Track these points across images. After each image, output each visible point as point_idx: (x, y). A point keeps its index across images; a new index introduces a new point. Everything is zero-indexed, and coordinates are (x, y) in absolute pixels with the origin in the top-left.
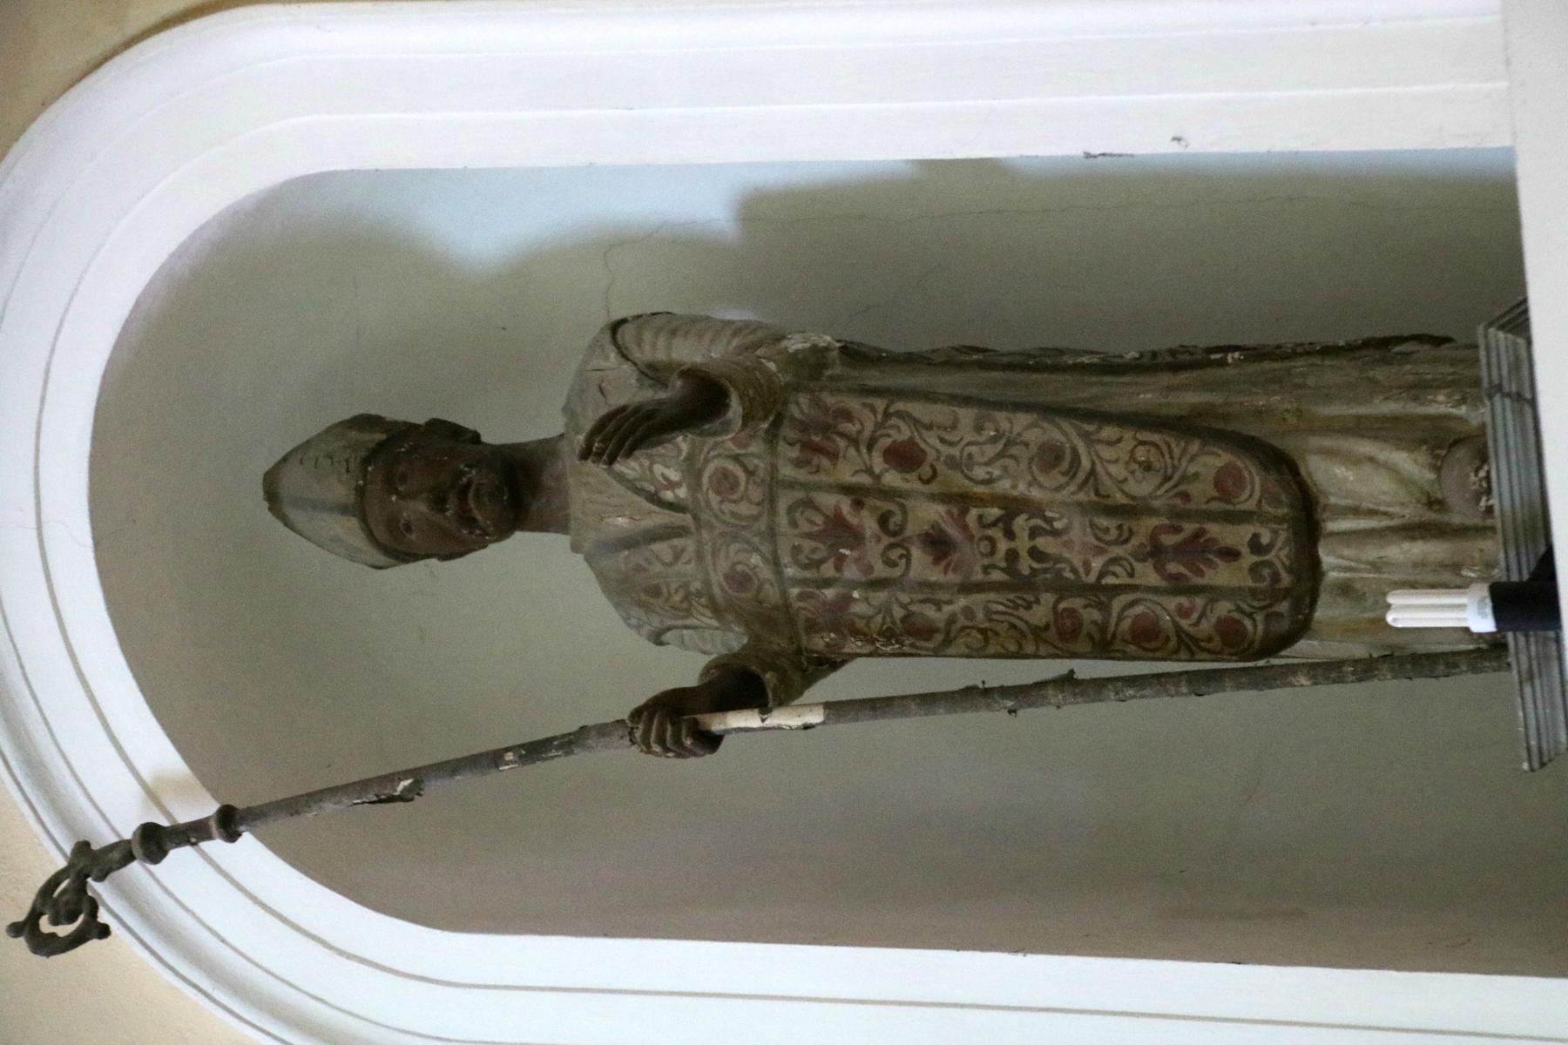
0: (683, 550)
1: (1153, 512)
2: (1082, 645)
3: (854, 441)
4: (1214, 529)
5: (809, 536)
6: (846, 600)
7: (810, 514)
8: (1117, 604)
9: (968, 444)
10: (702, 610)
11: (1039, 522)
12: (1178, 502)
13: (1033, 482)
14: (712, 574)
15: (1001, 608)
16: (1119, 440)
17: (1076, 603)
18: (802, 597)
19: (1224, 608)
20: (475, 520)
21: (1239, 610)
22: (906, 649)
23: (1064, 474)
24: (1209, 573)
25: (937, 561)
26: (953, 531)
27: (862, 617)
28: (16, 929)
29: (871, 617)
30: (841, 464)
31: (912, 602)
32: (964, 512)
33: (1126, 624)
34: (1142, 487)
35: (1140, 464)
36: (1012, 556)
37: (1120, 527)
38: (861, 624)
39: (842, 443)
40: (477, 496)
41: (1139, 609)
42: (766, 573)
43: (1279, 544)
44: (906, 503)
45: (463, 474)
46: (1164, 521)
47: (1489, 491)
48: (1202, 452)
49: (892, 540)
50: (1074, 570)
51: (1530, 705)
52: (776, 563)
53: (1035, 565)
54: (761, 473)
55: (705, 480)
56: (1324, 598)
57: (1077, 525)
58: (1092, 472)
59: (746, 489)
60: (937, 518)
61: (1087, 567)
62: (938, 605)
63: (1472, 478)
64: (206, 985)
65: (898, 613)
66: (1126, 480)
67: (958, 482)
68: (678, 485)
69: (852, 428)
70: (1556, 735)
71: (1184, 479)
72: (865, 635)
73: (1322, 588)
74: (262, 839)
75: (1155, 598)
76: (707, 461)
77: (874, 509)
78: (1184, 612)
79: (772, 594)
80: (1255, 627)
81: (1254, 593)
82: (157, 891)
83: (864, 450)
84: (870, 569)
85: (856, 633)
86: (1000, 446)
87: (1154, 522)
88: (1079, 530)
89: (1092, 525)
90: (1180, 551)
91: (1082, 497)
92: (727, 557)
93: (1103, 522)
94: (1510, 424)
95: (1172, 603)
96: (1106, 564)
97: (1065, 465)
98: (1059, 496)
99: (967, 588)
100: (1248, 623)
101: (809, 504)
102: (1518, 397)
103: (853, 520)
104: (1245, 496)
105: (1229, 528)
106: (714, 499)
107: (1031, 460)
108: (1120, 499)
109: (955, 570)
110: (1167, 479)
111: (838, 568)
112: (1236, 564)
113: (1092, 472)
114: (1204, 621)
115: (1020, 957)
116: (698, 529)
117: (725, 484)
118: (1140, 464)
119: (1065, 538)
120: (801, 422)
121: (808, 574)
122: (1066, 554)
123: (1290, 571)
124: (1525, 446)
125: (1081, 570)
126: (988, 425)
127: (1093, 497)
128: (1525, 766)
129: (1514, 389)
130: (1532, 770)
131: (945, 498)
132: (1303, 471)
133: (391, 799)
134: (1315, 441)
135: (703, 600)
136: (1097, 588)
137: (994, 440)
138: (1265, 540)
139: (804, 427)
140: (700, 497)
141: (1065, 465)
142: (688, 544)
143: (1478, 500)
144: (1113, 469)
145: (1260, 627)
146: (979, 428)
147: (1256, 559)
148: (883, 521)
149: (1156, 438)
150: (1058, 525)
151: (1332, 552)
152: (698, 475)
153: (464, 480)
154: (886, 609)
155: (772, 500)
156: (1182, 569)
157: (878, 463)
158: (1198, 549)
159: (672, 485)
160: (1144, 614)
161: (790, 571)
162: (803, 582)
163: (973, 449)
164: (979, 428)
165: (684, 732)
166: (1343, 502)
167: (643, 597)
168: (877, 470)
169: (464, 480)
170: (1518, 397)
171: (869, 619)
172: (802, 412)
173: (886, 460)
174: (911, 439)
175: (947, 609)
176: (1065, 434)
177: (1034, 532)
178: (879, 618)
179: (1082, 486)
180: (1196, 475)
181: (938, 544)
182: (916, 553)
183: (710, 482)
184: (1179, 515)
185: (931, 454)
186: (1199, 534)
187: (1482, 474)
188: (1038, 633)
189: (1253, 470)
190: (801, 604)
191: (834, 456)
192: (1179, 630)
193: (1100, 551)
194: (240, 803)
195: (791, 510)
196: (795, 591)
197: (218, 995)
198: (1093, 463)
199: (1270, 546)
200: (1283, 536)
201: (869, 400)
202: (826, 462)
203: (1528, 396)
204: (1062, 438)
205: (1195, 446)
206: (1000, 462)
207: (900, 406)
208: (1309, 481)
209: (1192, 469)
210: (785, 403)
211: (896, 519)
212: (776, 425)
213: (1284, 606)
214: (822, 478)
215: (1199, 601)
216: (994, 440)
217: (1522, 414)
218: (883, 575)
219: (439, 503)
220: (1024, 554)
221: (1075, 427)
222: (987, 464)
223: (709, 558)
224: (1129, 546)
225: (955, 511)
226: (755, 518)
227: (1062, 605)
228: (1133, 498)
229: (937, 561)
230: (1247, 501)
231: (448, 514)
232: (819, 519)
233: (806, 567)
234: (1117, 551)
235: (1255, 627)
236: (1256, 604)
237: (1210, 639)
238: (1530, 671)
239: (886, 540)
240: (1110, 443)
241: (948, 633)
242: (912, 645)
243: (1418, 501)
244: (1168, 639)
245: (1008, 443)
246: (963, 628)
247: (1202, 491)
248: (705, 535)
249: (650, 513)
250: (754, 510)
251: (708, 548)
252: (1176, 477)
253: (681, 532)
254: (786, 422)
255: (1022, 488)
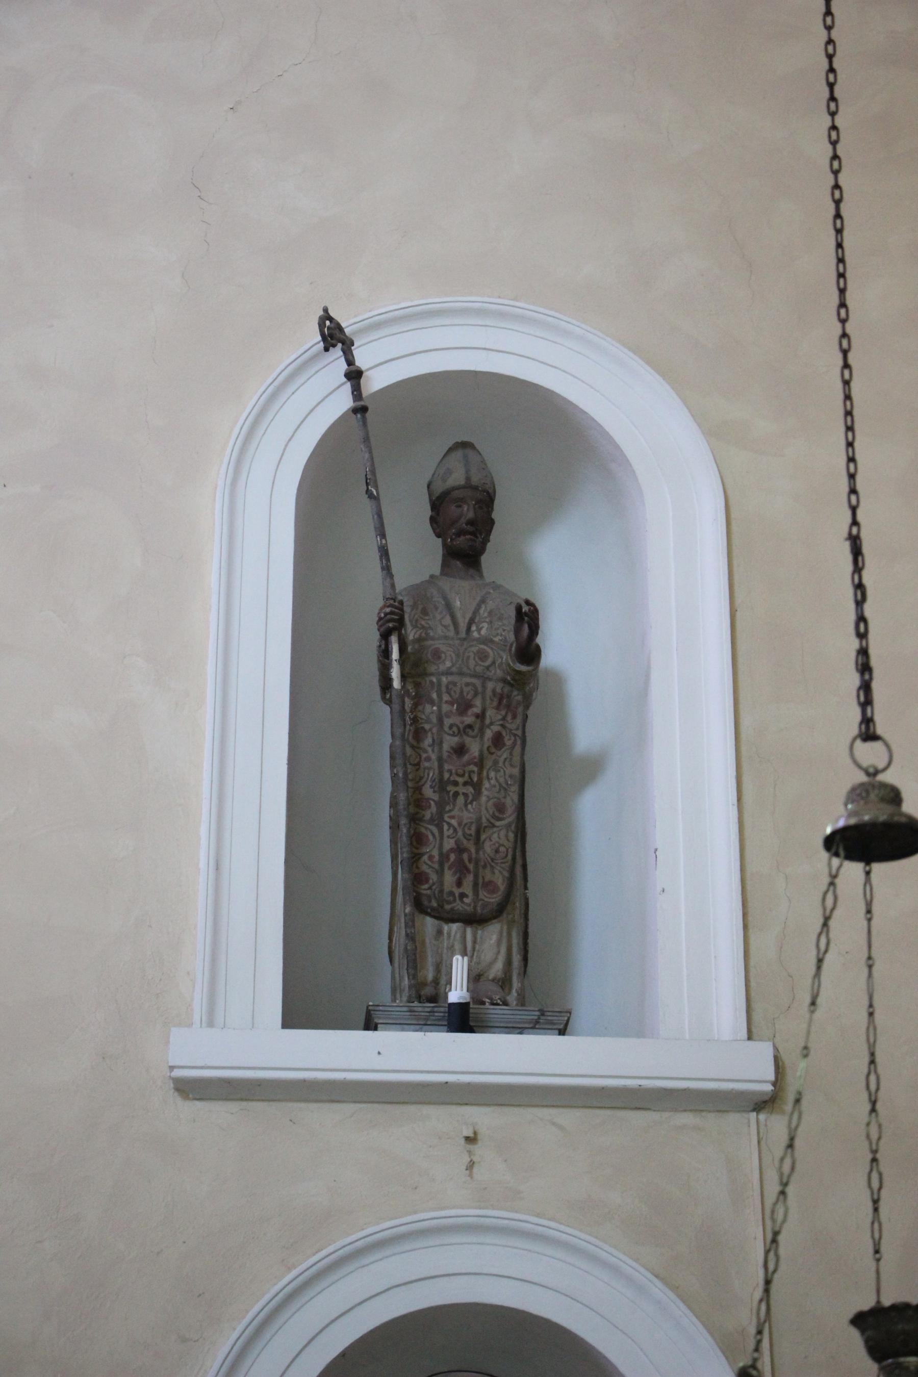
1: (477, 852)
2: (412, 809)
3: (504, 719)
4: (470, 878)
5: (462, 692)
6: (432, 703)
8: (435, 830)
10: (418, 633)
11: (471, 798)
12: (483, 864)
13: (489, 799)
15: (431, 775)
17: (434, 809)
19: (434, 877)
20: (459, 536)
21: (434, 884)
22: (408, 727)
24: (451, 872)
25: (452, 748)
26: (466, 758)
28: (326, 310)
29: (424, 713)
30: (494, 711)
32: (475, 764)
33: (423, 830)
34: (488, 848)
36: (456, 784)
37: (471, 835)
38: (420, 708)
39: (503, 713)
40: (471, 540)
41: (431, 837)
42: (442, 668)
45: (481, 534)
46: (474, 856)
50: (450, 811)
51: (398, 1009)
52: (448, 673)
53: (451, 793)
54: (488, 673)
55: (482, 646)
56: (436, 922)
57: (471, 815)
58: (494, 826)
61: (452, 817)
62: (432, 745)
64: (276, 383)
65: (427, 727)
67: (488, 763)
68: (479, 632)
69: (509, 718)
75: (437, 846)
76: (492, 649)
78: (431, 858)
81: (441, 891)
82: (316, 368)
83: (501, 722)
84: (448, 717)
86: (504, 785)
87: (473, 850)
88: (468, 816)
89: (472, 823)
90: (460, 861)
93: (473, 828)
95: (435, 853)
97: (497, 814)
98: (483, 809)
99: (440, 760)
100: (426, 886)
102: (537, 1022)
103: (470, 712)
105: (471, 884)
106: (475, 649)
107: (499, 799)
108: (483, 837)
109: (449, 756)
110: (493, 860)
112: (454, 885)
113: (494, 826)
116: (460, 639)
117: (483, 656)
121: (444, 689)
122: (456, 809)
123: (452, 909)
128: (371, 1003)
131: (482, 758)
133: (367, 484)
134: (505, 927)
135: (423, 635)
136: (442, 819)
138: (465, 900)
139: (509, 697)
141: (497, 814)
142: (452, 633)
144: (495, 835)
145: (424, 892)
146: (511, 776)
147: (457, 895)
148: (470, 727)
150: (469, 806)
152: (484, 643)
154: (428, 721)
155: (475, 675)
157: (496, 728)
158: (461, 869)
159: (479, 630)
160: (429, 840)
161: (444, 680)
162: (439, 684)
164: (511, 776)
167: (420, 607)
170: (537, 1022)
175: (430, 749)
178: (423, 717)
179: (488, 820)
180: (494, 873)
181: (460, 750)
185: (499, 753)
186: (468, 871)
191: (498, 708)
192: (422, 855)
193: (460, 824)
195: (474, 685)
196: (434, 680)
197: (272, 387)
199: (463, 902)
201: (521, 728)
207: (519, 742)
209: (496, 871)
210: (518, 690)
211: (470, 732)
212: (509, 683)
214: (488, 702)
215: (436, 866)
216: (507, 784)
217: (530, 1023)
219: (471, 523)
220: (456, 789)
222: (496, 778)
224: (462, 838)
226: (468, 668)
227: (432, 803)
229: (452, 748)
230: (483, 894)
232: (469, 697)
233: (447, 687)
234: (460, 833)
237: (417, 867)
239: (461, 726)
240: (507, 836)
241: (419, 748)
244: (417, 849)
245: (505, 789)
248: (457, 642)
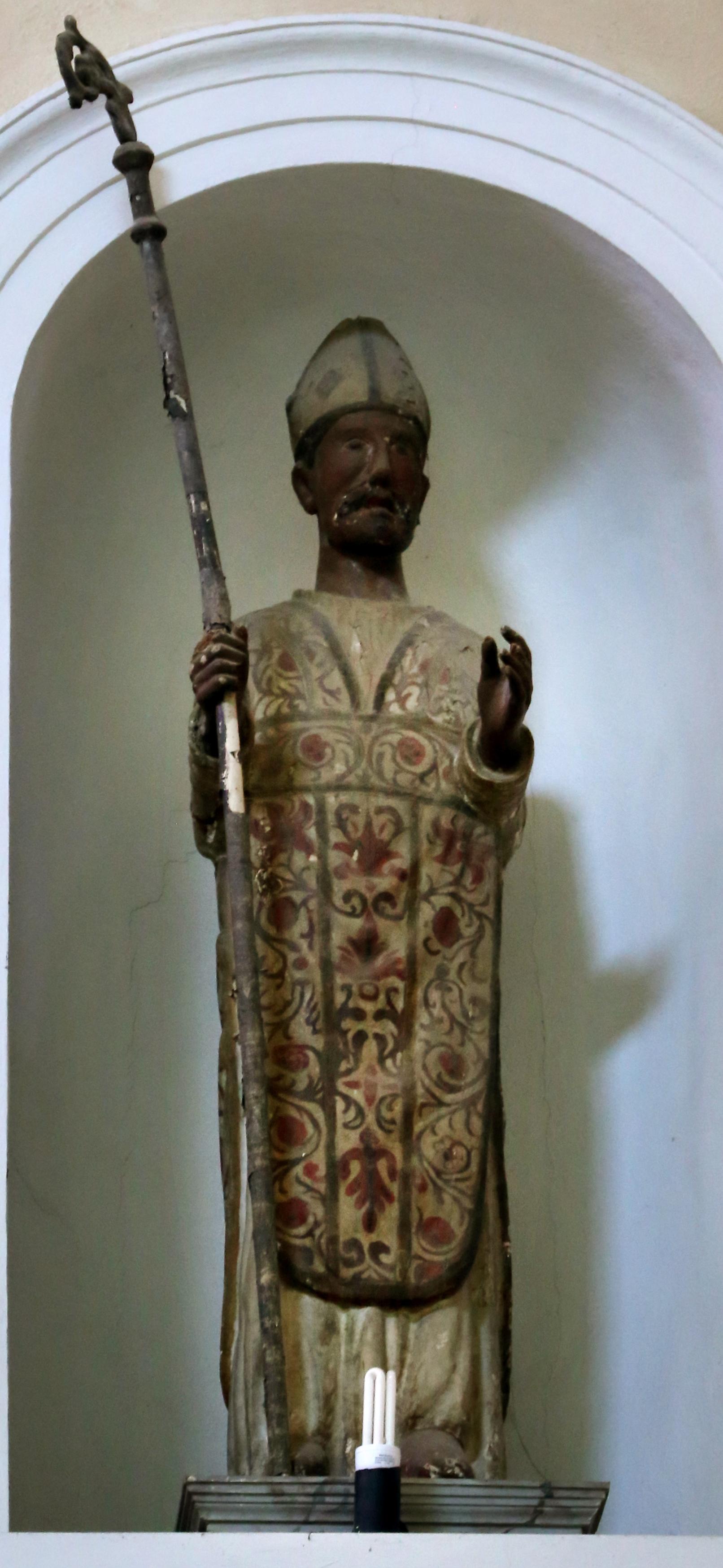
0: (337, 699)
1: (407, 1156)
2: (271, 1069)
3: (457, 881)
4: (392, 1212)
5: (369, 825)
6: (308, 849)
7: (389, 830)
9: (461, 991)
11: (391, 1045)
12: (418, 1181)
13: (429, 1047)
14: (318, 724)
15: (307, 996)
16: (470, 1132)
18: (305, 806)
19: (317, 1210)
21: (317, 1224)
23: (439, 1076)
25: (351, 941)
26: (380, 961)
27: (290, 859)
31: (309, 911)
32: (400, 975)
34: (429, 1148)
36: (359, 1015)
37: (393, 1122)
38: (282, 857)
39: (456, 869)
45: (403, 506)
46: (399, 1165)
47: (443, 1475)
48: (463, 1209)
49: (370, 901)
50: (349, 1072)
52: (339, 786)
53: (350, 1035)
54: (423, 788)
57: (392, 1081)
60: (390, 950)
62: (308, 935)
63: (454, 1462)
65: (297, 896)
67: (427, 974)
68: (403, 706)
69: (468, 880)
71: (438, 1190)
72: (271, 859)
73: (332, 1306)
75: (323, 1143)
76: (430, 738)
77: (397, 889)
78: (310, 1170)
79: (306, 777)
81: (333, 1240)
83: (451, 889)
84: (342, 877)
85: (272, 854)
88: (386, 1082)
89: (394, 1096)
91: (420, 1090)
92: (338, 741)
93: (398, 1107)
94: (512, 1502)
95: (320, 1159)
96: (356, 1104)
97: (446, 1078)
98: (418, 1067)
99: (326, 966)
100: (302, 1230)
101: (399, 830)
102: (538, 1512)
103: (386, 867)
106: (395, 738)
107: (449, 1046)
109: (343, 958)
110: (439, 1173)
111: (337, 846)
113: (440, 1104)
115: (5, 963)
116: (361, 718)
117: (412, 753)
119: (378, 1068)
120: (471, 834)
121: (331, 818)
122: (362, 1067)
123: (357, 1277)
124: (498, 1514)
127: (420, 1101)
130: (187, 1484)
131: (412, 959)
132: (444, 1302)
133: (167, 387)
137: (465, 1014)
138: (385, 1258)
139: (467, 837)
140: (393, 726)
141: (446, 1078)
142: (344, 705)
143: (435, 1464)
144: (443, 1125)
145: (298, 1242)
146: (474, 1001)
148: (388, 897)
149: (474, 1168)
150: (389, 1063)
151: (370, 1319)
153: (398, 507)
154: (300, 885)
155: (395, 792)
156: (352, 1177)
157: (441, 901)
158: (374, 1193)
159: (402, 701)
161: (332, 800)
162: (321, 809)
166: (411, 1336)
168: (433, 899)
169: (398, 507)
171: (288, 867)
172: (480, 836)
173: (442, 909)
174: (459, 936)
175: (304, 944)
176: (473, 1082)
177: (380, 1039)
178: (289, 876)
179: (428, 1090)
180: (441, 1201)
181: (367, 945)
182: (357, 924)
184: (406, 1178)
185: (448, 952)
186: (389, 1197)
187: (457, 1470)
189: (450, 1256)
190: (297, 804)
191: (443, 859)
193: (370, 1100)
194: (166, 244)
195: (392, 810)
196: (311, 800)
198: (448, 1105)
199: (378, 1262)
200: (389, 1275)
201: (492, 899)
203: (538, 1522)
205: (468, 1204)
208: (435, 1306)
209: (447, 1198)
210: (485, 822)
211: (389, 910)
212: (466, 809)
213: (319, 1267)
215: (322, 1187)
216: (465, 1014)
219: (381, 480)
220: (361, 1026)
221: (480, 1092)
223: (331, 723)
224: (375, 1128)
225: (401, 967)
226: (380, 774)
227: (311, 1055)
229: (351, 941)
232: (386, 836)
234: (370, 1118)
235: (297, 1237)
236: (323, 1241)
238: (283, 1494)
243: (419, 1406)
244: (282, 1151)
245: (464, 1029)
246: (284, 957)
249: (371, 675)
251: (344, 724)
252: (440, 1183)
253: (355, 701)
254: (470, 821)
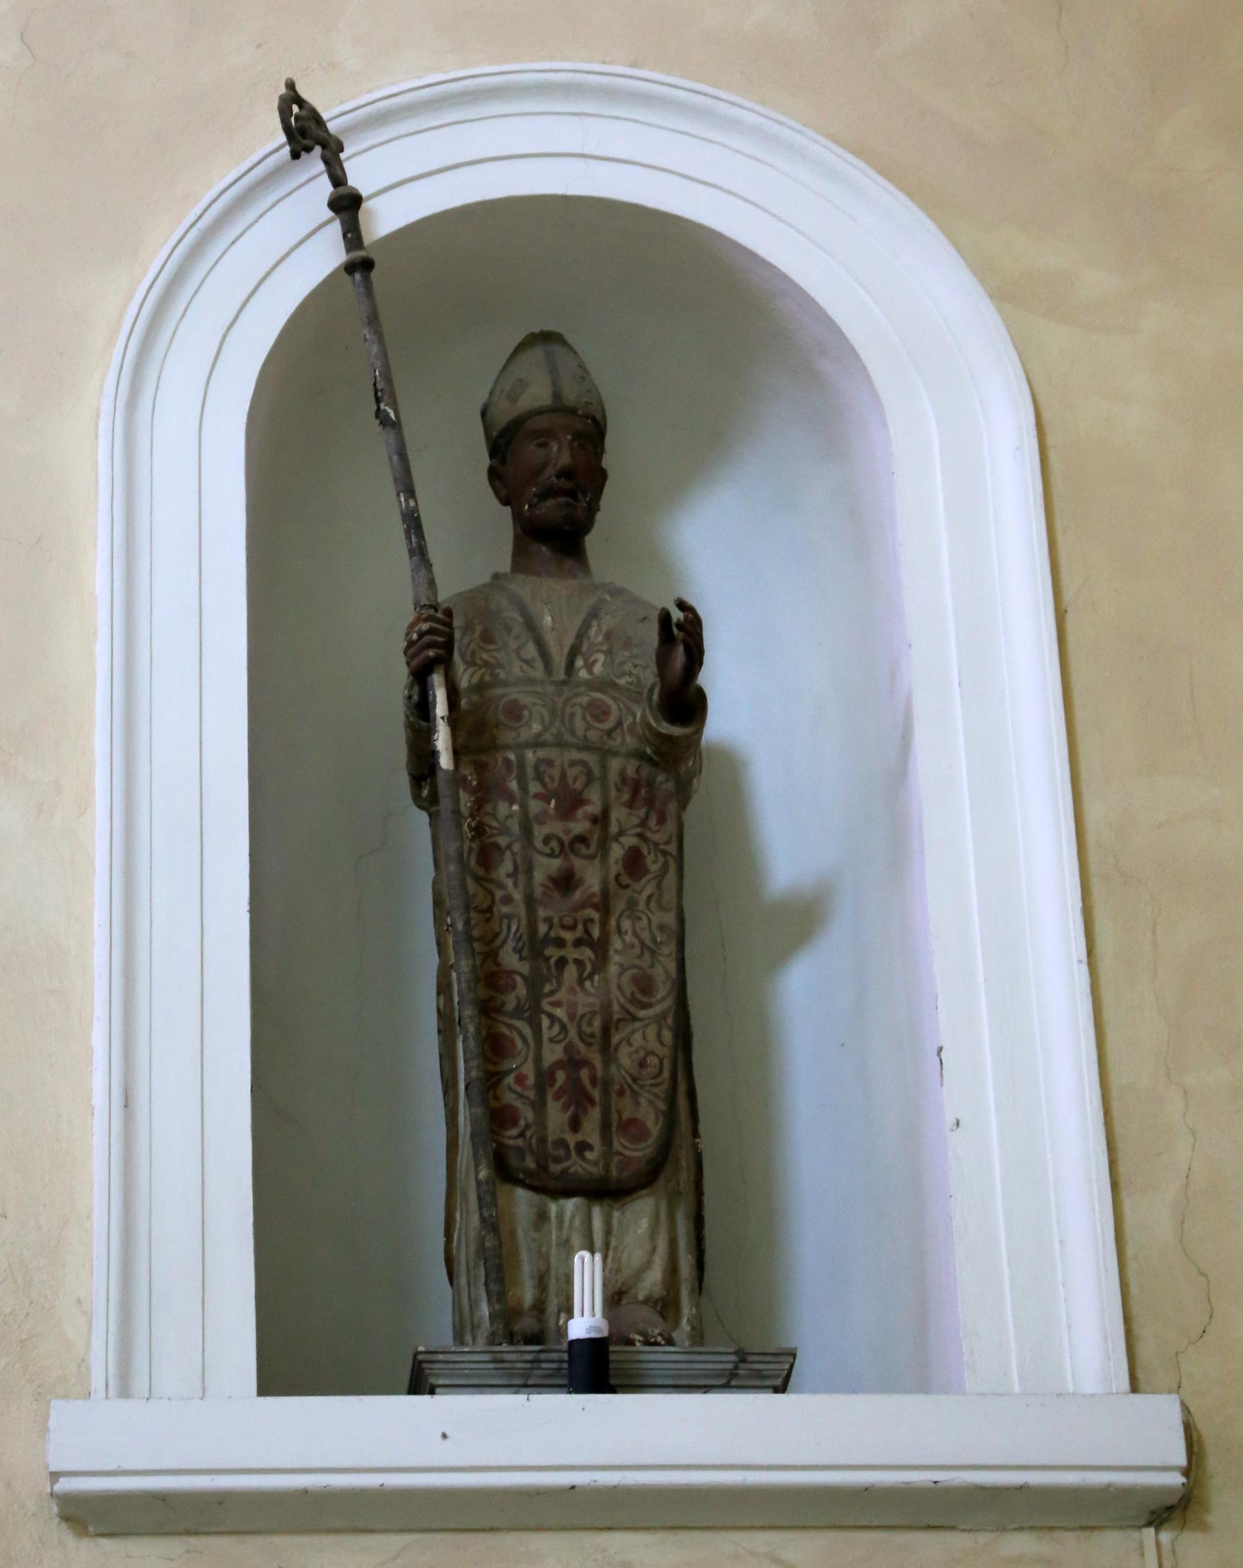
0: (533, 667)
1: (606, 1064)
2: (483, 992)
3: (643, 823)
4: (595, 1114)
5: (563, 776)
6: (511, 799)
9: (649, 919)
11: (589, 968)
12: (617, 1087)
13: (623, 969)
15: (514, 928)
16: (662, 1043)
17: (522, 990)
18: (507, 762)
19: (527, 1114)
21: (527, 1126)
23: (632, 994)
25: (552, 879)
26: (577, 896)
27: (495, 809)
30: (625, 811)
31: (513, 854)
32: (595, 907)
34: (625, 1058)
35: (644, 1059)
36: (560, 943)
37: (592, 1035)
38: (488, 808)
39: (642, 812)
40: (568, 504)
43: (585, 1165)
44: (598, 860)
45: (585, 495)
46: (600, 1073)
49: (566, 843)
50: (552, 993)
52: (537, 744)
53: (553, 961)
54: (611, 742)
55: (598, 695)
57: (591, 1000)
58: (635, 1019)
59: (597, 729)
62: (513, 875)
63: (657, 1331)
65: (503, 841)
66: (630, 1045)
67: (619, 905)
68: (590, 671)
69: (653, 822)
70: (444, 1376)
71: (635, 1095)
72: (478, 810)
73: (543, 1197)
74: (329, 283)
75: (531, 1056)
76: (615, 699)
78: (520, 1079)
79: (507, 737)
80: (510, 1138)
81: (543, 1140)
83: (638, 830)
85: (479, 804)
88: (586, 1000)
89: (593, 1013)
90: (575, 1083)
91: (616, 1008)
93: (597, 1023)
94: (710, 1366)
95: (529, 1070)
96: (560, 1021)
97: (639, 996)
98: (614, 988)
99: (530, 901)
101: (590, 780)
102: (733, 1375)
103: (580, 813)
104: (623, 1141)
106: (584, 700)
107: (641, 968)
108: (615, 1039)
109: (545, 894)
110: (635, 1080)
111: (536, 796)
112: (567, 1128)
113: (635, 1019)
114: (513, 1096)
117: (599, 712)
118: (644, 1059)
119: (578, 989)
121: (530, 772)
122: (564, 988)
123: (564, 1172)
125: (552, 999)
126: (665, 936)
127: (616, 1017)
129: (740, 1372)
130: (417, 1353)
131: (605, 893)
132: (644, 1192)
138: (589, 1155)
139: (650, 784)
140: (582, 689)
141: (639, 996)
142: (539, 672)
143: (640, 1333)
144: (638, 1036)
145: (511, 1142)
146: (662, 928)
147: (572, 1146)
148: (582, 839)
150: (588, 984)
154: (504, 831)
155: (586, 747)
156: (558, 1084)
157: (630, 841)
158: (578, 1099)
159: (589, 666)
161: (530, 756)
163: (645, 920)
165: (439, 651)
166: (615, 1222)
167: (479, 629)
168: (622, 839)
170: (733, 1375)
171: (494, 816)
172: (661, 783)
173: (630, 848)
174: (647, 871)
175: (509, 883)
177: (579, 963)
179: (623, 1007)
180: (638, 1104)
181: (566, 882)
182: (556, 863)
183: (600, 700)
184: (606, 1085)
186: (591, 1101)
187: (659, 1339)
188: (491, 955)
189: (648, 1151)
190: (500, 760)
191: (630, 805)
193: (571, 1017)
194: (375, 275)
195: (583, 763)
198: (642, 1020)
201: (674, 839)
202: (626, 797)
203: (733, 1383)
204: (659, 996)
205: (662, 1106)
206: (636, 941)
207: (673, 867)
209: (642, 1100)
211: (583, 849)
212: (649, 760)
213: (530, 1163)
214: (613, 793)
215: (531, 1094)
216: (654, 940)
218: (536, 833)
219: (565, 473)
220: (562, 953)
224: (577, 1041)
225: (596, 900)
226: (572, 731)
227: (518, 979)
228: (616, 1049)
229: (552, 879)
230: (619, 1142)
231: (553, 478)
233: (536, 768)
234: (573, 1032)
235: (510, 1138)
238: (503, 1361)
239: (566, 839)
240: (659, 1036)
241: (484, 879)
242: (471, 849)
244: (495, 1064)
245: (653, 953)
246: (492, 894)
247: (626, 1108)
250: (580, 732)
251: (539, 689)
252: (636, 1088)
255: (616, 958)
